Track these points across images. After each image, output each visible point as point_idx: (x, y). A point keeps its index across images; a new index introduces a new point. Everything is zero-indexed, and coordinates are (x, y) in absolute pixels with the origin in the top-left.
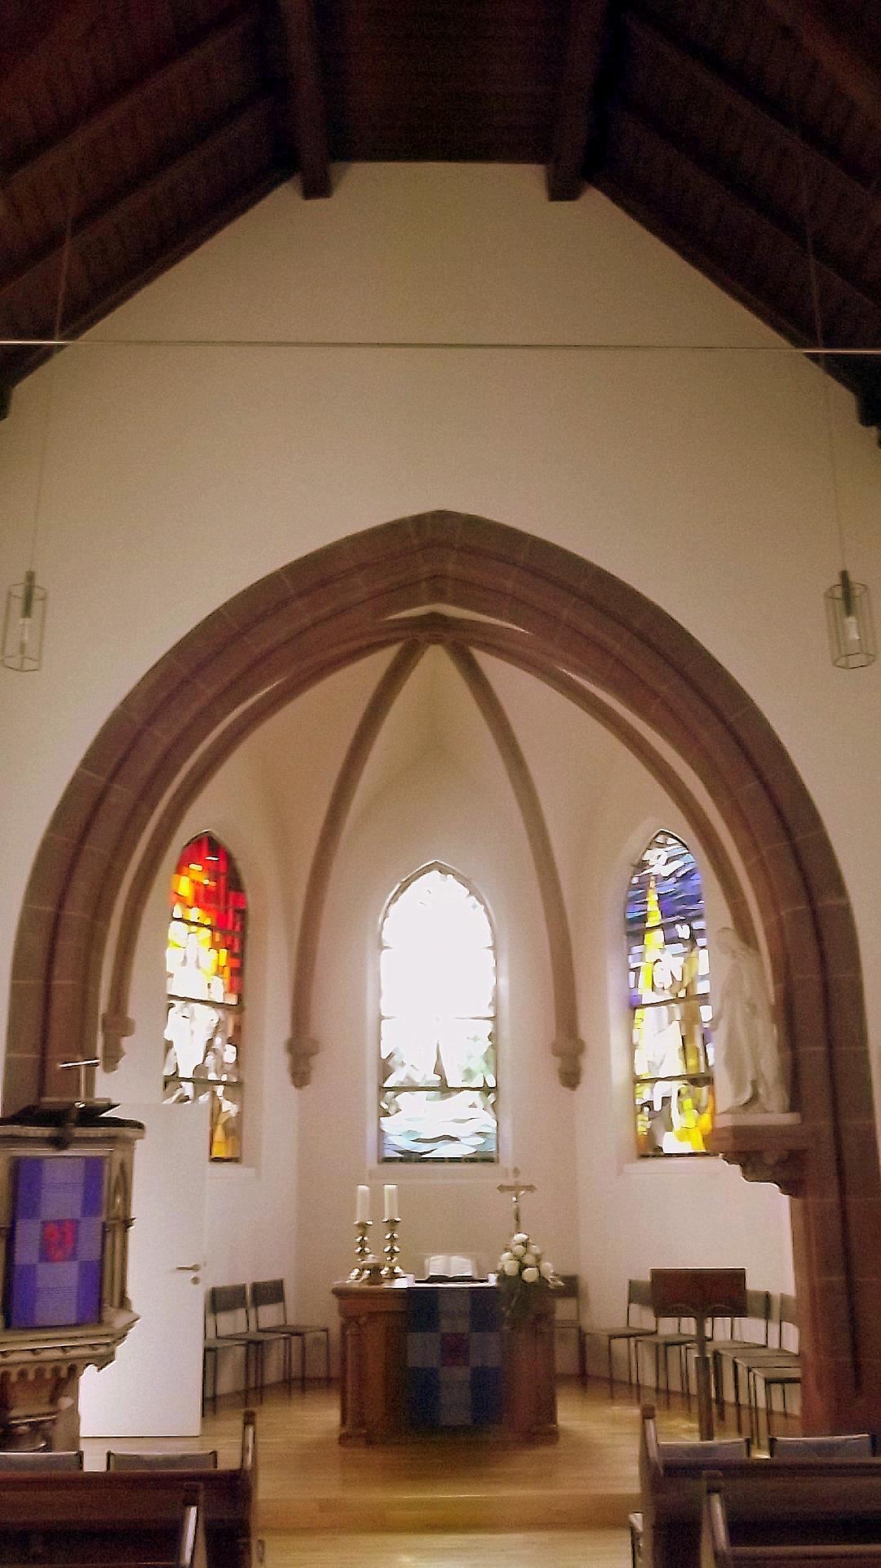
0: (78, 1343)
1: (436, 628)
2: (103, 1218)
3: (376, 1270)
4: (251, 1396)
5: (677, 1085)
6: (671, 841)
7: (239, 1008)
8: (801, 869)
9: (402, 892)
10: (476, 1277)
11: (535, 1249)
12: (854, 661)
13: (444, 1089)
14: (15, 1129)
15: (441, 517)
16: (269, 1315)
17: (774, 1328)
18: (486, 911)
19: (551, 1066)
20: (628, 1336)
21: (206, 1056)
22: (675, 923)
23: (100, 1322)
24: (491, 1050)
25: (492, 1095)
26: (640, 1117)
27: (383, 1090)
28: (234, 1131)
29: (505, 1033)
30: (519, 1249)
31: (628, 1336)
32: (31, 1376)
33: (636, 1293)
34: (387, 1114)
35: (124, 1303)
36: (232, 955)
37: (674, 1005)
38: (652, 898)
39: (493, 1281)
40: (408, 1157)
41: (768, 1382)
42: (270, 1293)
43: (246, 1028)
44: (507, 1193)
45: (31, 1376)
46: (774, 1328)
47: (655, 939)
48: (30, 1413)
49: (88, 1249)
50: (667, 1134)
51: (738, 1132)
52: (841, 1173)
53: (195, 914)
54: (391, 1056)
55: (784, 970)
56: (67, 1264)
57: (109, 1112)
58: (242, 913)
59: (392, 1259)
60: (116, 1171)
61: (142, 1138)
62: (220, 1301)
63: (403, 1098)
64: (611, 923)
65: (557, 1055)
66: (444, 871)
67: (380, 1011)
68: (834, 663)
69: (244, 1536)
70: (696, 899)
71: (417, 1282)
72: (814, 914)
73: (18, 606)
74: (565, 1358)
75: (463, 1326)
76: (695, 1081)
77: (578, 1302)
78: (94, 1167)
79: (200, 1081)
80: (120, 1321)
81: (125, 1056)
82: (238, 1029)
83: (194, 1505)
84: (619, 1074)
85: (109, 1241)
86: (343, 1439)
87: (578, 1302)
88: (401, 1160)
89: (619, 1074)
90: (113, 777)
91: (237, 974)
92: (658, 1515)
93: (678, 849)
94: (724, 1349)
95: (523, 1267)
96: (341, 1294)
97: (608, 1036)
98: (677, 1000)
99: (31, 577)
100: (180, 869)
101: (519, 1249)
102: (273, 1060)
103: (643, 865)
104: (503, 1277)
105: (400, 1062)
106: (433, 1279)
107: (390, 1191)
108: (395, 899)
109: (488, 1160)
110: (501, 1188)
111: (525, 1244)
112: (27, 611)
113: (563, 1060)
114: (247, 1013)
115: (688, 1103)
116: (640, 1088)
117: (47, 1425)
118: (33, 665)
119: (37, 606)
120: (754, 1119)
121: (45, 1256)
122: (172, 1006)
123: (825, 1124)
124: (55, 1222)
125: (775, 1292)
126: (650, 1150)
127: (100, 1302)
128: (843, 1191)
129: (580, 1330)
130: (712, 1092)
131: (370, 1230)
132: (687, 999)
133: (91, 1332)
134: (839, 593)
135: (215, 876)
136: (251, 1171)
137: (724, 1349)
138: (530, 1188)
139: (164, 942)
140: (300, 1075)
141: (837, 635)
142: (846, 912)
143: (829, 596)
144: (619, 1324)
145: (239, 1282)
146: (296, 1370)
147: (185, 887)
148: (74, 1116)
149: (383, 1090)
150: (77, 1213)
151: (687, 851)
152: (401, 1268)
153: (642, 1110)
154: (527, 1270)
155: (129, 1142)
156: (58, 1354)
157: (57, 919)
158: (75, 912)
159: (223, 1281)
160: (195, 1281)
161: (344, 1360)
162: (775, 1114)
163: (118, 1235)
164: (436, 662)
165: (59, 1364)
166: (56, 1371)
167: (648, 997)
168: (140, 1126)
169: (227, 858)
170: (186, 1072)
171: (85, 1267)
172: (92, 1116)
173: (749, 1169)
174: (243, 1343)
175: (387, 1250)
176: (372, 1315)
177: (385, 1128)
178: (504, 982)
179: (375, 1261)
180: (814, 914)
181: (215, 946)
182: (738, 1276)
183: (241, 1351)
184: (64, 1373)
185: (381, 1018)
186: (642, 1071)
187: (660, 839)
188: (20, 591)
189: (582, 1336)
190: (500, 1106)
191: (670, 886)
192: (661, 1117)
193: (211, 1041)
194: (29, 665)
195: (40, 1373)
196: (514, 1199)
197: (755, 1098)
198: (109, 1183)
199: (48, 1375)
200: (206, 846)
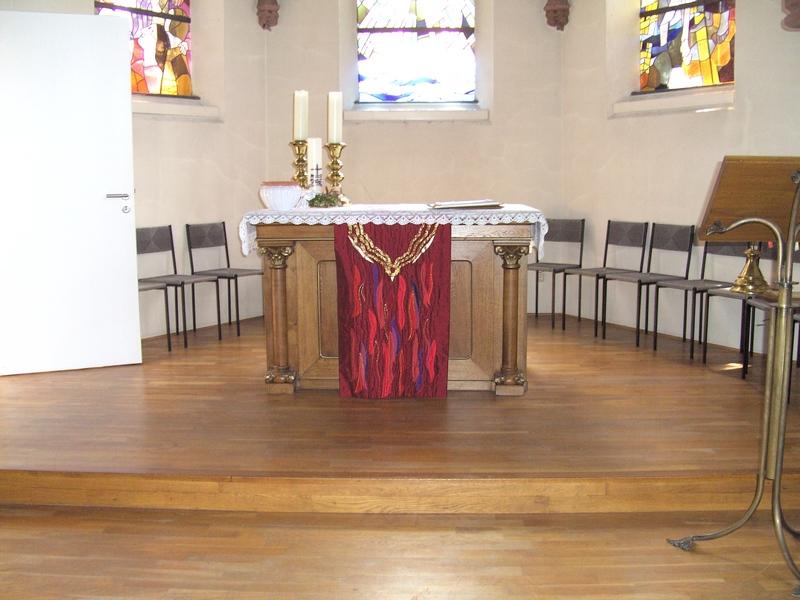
26: (643, 54)
62: (152, 240)
115: (701, 34)
160: (125, 210)
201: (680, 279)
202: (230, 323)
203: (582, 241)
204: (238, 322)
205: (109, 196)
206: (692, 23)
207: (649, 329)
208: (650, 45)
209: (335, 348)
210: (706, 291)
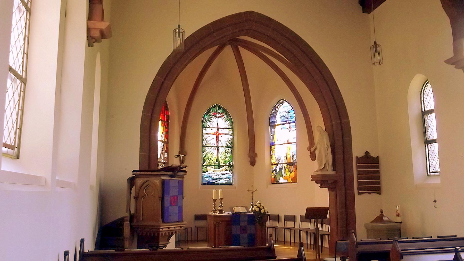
13: (219, 166)
15: (251, 13)
19: (248, 160)
26: (272, 173)
27: (203, 166)
30: (259, 205)
34: (204, 172)
36: (166, 128)
40: (210, 183)
54: (205, 156)
58: (168, 117)
63: (209, 168)
75: (246, 224)
82: (167, 148)
87: (207, 220)
88: (208, 184)
89: (267, 163)
90: (165, 79)
101: (259, 205)
102: (292, 157)
104: (255, 211)
106: (236, 213)
107: (220, 191)
111: (260, 204)
115: (287, 170)
116: (272, 166)
121: (171, 204)
123: (342, 174)
126: (275, 182)
149: (203, 166)
153: (273, 172)
162: (330, 172)
164: (228, 51)
176: (222, 221)
184: (171, 234)
186: (273, 161)
191: (284, 114)
199: (167, 234)
206: (285, 167)
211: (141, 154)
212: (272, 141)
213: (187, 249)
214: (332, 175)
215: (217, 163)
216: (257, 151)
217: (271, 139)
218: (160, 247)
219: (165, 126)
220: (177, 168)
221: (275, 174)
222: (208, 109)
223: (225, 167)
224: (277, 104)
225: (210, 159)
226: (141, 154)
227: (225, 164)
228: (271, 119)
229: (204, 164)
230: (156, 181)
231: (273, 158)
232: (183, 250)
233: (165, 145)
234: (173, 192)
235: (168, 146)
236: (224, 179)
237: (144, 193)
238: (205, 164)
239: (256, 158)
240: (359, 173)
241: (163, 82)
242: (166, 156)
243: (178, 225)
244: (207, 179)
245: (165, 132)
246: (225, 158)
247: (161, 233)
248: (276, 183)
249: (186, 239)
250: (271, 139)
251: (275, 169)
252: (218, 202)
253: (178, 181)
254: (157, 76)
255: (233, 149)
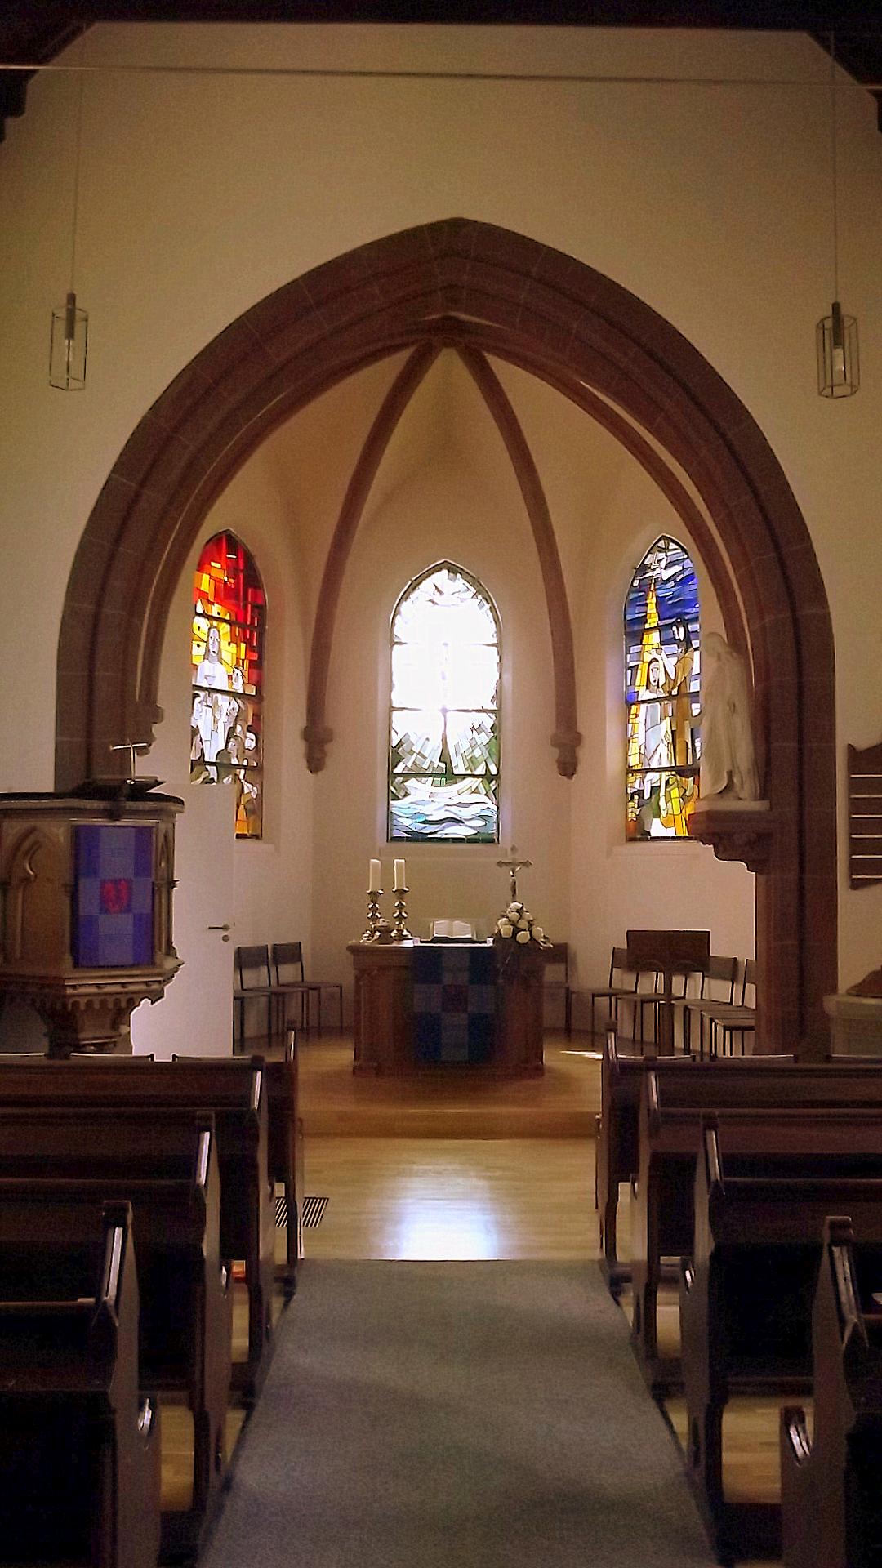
0: (135, 981)
1: (450, 332)
2: (153, 879)
3: (386, 931)
4: (274, 1039)
5: (665, 776)
6: (672, 546)
7: (258, 698)
8: (786, 578)
9: (414, 589)
10: (475, 939)
11: (528, 916)
12: (838, 391)
13: (449, 776)
14: (75, 802)
15: (457, 226)
16: (288, 973)
17: (738, 988)
18: (492, 609)
20: (610, 995)
21: (228, 742)
22: (672, 625)
23: (153, 963)
24: (494, 740)
25: (494, 782)
26: (631, 804)
28: (255, 810)
29: (508, 725)
31: (610, 995)
32: (97, 1006)
33: (617, 959)
34: (396, 798)
35: (170, 951)
36: (250, 648)
37: (666, 702)
38: (652, 602)
39: (490, 942)
40: (415, 837)
41: (725, 1028)
42: (288, 953)
43: (265, 715)
44: (504, 867)
45: (97, 1006)
46: (738, 988)
47: (654, 638)
48: (97, 1036)
49: (141, 902)
50: (655, 820)
51: (711, 816)
52: (802, 855)
53: (215, 610)
54: (400, 743)
55: (764, 672)
56: (124, 916)
57: (156, 788)
58: (260, 609)
59: (400, 923)
60: (161, 839)
61: (182, 812)
62: (245, 959)
63: (412, 783)
64: (612, 625)
65: (554, 745)
66: (453, 570)
67: (390, 700)
68: (820, 394)
69: (289, 1109)
70: (692, 602)
71: (421, 942)
72: (796, 622)
73: (61, 327)
74: (552, 1014)
75: (463, 978)
76: (682, 772)
77: (567, 965)
78: (143, 834)
79: (223, 764)
80: (169, 964)
81: (156, 742)
82: (257, 717)
83: (259, 1070)
84: (613, 765)
85: (157, 897)
86: (356, 1070)
87: (567, 965)
89: (613, 765)
90: (142, 484)
91: (256, 666)
92: (613, 1101)
93: (679, 554)
94: (693, 1005)
95: (517, 930)
96: (355, 950)
97: (604, 729)
98: (670, 697)
99: (72, 298)
100: (201, 567)
103: (644, 568)
104: (498, 938)
105: (408, 750)
108: (405, 596)
109: (489, 841)
110: (500, 864)
111: (520, 911)
112: (70, 335)
113: (560, 752)
114: (265, 703)
115: (675, 793)
117: (111, 1046)
118: (77, 385)
119: (79, 327)
120: (729, 805)
121: (104, 910)
122: (198, 695)
123: (791, 811)
124: (111, 881)
125: (742, 959)
126: (639, 834)
127: (153, 948)
128: (802, 869)
129: (567, 989)
130: (697, 782)
131: (380, 898)
132: (677, 696)
133: (146, 971)
134: (829, 324)
135: (232, 570)
136: (270, 847)
137: (693, 1005)
138: (526, 864)
139: (189, 636)
140: (315, 763)
141: (825, 364)
142: (825, 621)
143: (821, 327)
144: (602, 984)
145: (263, 944)
146: (313, 1022)
147: (206, 584)
148: (125, 791)
149: (392, 775)
150: (129, 874)
151: (686, 556)
152: (408, 931)
153: (632, 798)
154: (520, 934)
155: (172, 815)
156: (118, 989)
157: (96, 617)
158: (112, 610)
159: (247, 943)
160: (225, 938)
161: (357, 1013)
162: (746, 801)
163: (164, 896)
164: (448, 367)
165: (118, 996)
166: (117, 1002)
167: (645, 694)
168: (181, 802)
169: (248, 558)
170: (210, 756)
171: (138, 919)
172: (140, 791)
173: (721, 848)
174: (268, 994)
175: (395, 915)
177: (393, 810)
178: (507, 677)
179: (385, 924)
180: (796, 622)
181: (234, 640)
182: (702, 939)
183: (264, 1000)
184: (123, 1005)
185: (392, 709)
186: (633, 761)
187: (662, 544)
188: (62, 313)
189: (569, 993)
190: (501, 793)
192: (648, 803)
193: (232, 730)
194: (73, 384)
195: (103, 1003)
196: (511, 873)
197: (729, 787)
198: (157, 849)
200: (226, 543)
201: (632, 992)
202: (278, 1033)
203: (566, 962)
204: (308, 1028)
205: (210, 928)
206: (667, 782)
207: (646, 1038)
208: (636, 797)
209: (847, 323)
210: (613, 995)
211: (59, 739)
212: (631, 689)
213: (171, 1060)
214: (759, 813)
215: (443, 765)
216: (582, 727)
217: (629, 684)
218: (85, 1045)
219: (248, 642)
220: (120, 787)
221: (638, 807)
222: (414, 579)
223: (469, 780)
224: (647, 555)
225: (419, 753)
226: (59, 739)
227: (469, 772)
228: (629, 610)
229: (396, 771)
230: (55, 830)
231: (633, 748)
232: (695, 1063)
233: (247, 707)
234: (116, 862)
235: (260, 709)
236: (466, 822)
237: (25, 869)
238: (398, 770)
239: (577, 749)
240: (855, 806)
241: (138, 495)
242: (250, 743)
243: (137, 976)
244: (406, 822)
245: (246, 663)
246: (471, 749)
247: (72, 1000)
248: (640, 840)
249: (305, 1025)
250: (629, 684)
251: (637, 787)
252: (388, 904)
253: (133, 832)
254: (113, 475)
255: (500, 716)
